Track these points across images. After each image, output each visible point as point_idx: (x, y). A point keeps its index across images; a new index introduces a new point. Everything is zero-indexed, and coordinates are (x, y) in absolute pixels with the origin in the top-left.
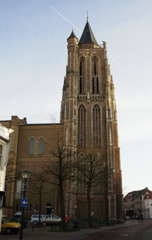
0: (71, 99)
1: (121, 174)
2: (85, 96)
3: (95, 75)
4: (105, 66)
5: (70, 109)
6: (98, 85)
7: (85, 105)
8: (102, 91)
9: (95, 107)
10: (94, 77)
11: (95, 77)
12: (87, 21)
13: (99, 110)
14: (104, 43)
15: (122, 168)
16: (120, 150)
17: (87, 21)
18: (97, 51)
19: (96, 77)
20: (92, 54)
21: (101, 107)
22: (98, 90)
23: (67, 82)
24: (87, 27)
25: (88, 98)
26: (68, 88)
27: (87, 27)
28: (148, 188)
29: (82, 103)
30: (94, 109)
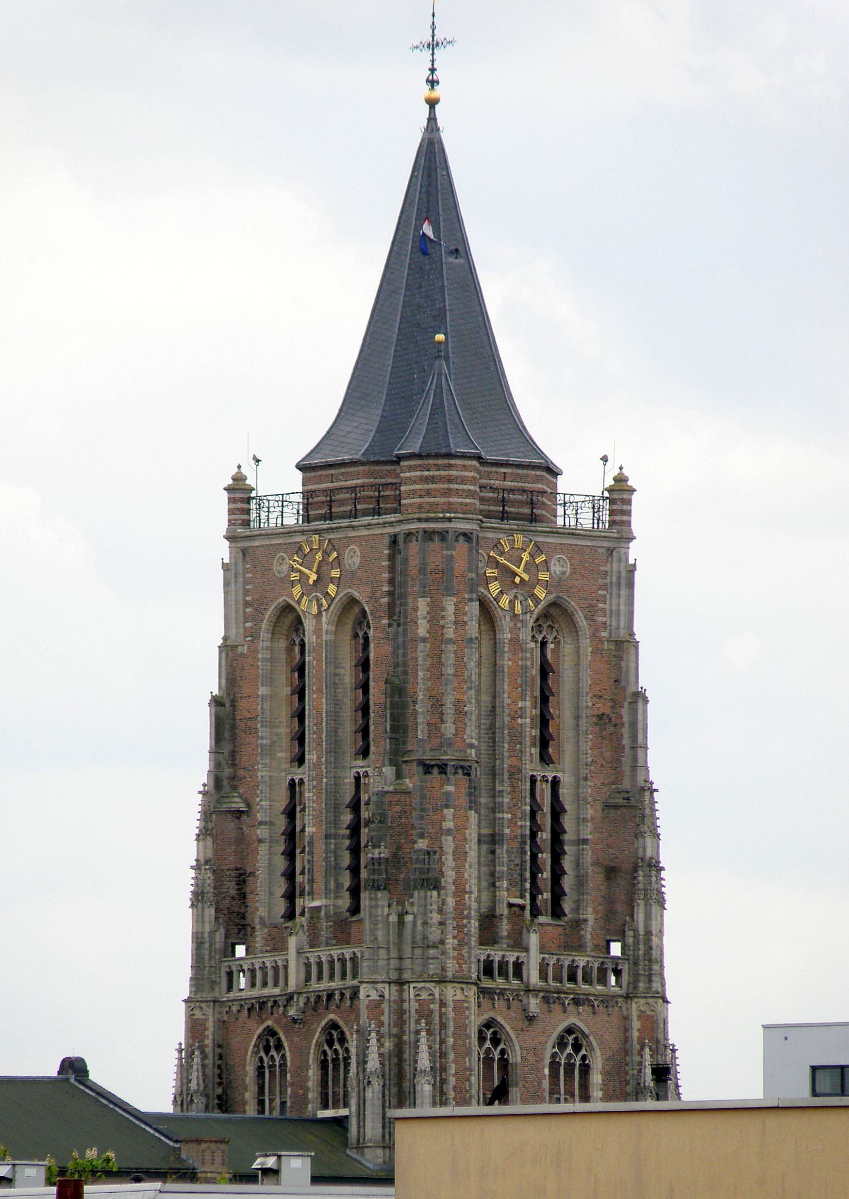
0: (459, 997)
1: (198, 898)
2: (512, 957)
3: (545, 758)
4: (616, 704)
5: (452, 1068)
6: (557, 855)
7: (508, 1029)
8: (596, 912)
9: (561, 1043)
10: (539, 775)
11: (544, 779)
12: (432, 119)
13: (585, 1069)
14: (620, 494)
15: (664, 943)
16: (639, 577)
17: (432, 119)
18: (571, 551)
19: (550, 776)
20: (546, 585)
21: (598, 1053)
22: (558, 894)
23: (422, 844)
24: (431, 182)
25: (533, 976)
26: (435, 893)
27: (431, 182)
28: (96, 1075)
29: (491, 1014)
30: (554, 1066)
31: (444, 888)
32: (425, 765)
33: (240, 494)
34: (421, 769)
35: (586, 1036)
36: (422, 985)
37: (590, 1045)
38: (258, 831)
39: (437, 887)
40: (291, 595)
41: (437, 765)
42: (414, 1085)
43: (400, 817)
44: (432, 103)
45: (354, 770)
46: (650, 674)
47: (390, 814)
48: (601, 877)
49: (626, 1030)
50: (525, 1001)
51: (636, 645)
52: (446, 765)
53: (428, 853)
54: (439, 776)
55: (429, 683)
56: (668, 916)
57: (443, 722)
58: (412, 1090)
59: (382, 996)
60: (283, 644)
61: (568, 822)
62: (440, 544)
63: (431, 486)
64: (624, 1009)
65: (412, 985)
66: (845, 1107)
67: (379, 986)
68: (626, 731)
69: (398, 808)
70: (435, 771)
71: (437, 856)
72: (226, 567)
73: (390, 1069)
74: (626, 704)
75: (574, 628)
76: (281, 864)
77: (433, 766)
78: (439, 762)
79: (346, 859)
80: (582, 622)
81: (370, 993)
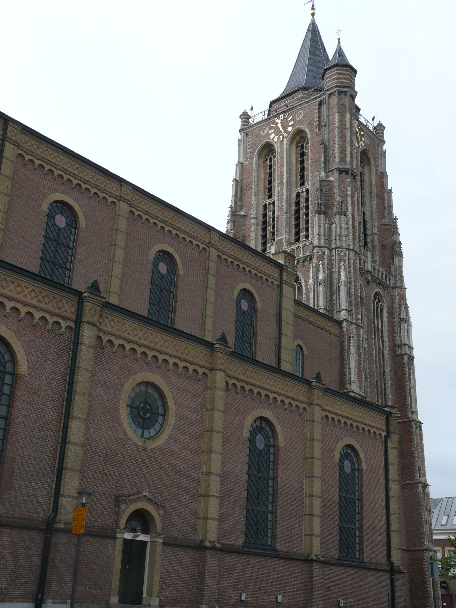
16: (387, 154)
21: (385, 305)
31: (348, 216)
32: (340, 170)
33: (245, 117)
34: (338, 172)
35: (382, 297)
36: (341, 249)
37: (383, 301)
38: (252, 221)
39: (345, 215)
40: (270, 139)
41: (345, 171)
42: (339, 287)
43: (329, 190)
44: (313, 15)
45: (296, 192)
46: (391, 184)
47: (324, 189)
48: (380, 247)
49: (393, 300)
50: (366, 275)
51: (387, 176)
52: (348, 171)
53: (342, 202)
54: (345, 175)
55: (341, 143)
56: (404, 260)
57: (346, 157)
58: (338, 289)
59: (324, 253)
60: (262, 161)
61: (369, 226)
62: (344, 96)
63: (341, 76)
64: (392, 292)
65: (337, 249)
66: (41, 530)
67: (322, 249)
68: (386, 202)
69: (327, 187)
70: (344, 173)
71: (345, 203)
72: (239, 140)
73: (340, 272)
74: (386, 193)
75: (369, 164)
76: (260, 233)
77: (343, 171)
78: (346, 170)
79: (293, 222)
80: (372, 162)
81: (319, 251)
